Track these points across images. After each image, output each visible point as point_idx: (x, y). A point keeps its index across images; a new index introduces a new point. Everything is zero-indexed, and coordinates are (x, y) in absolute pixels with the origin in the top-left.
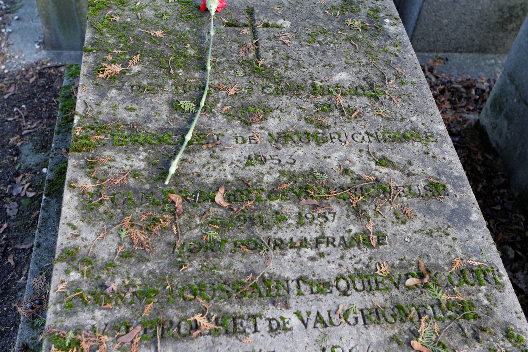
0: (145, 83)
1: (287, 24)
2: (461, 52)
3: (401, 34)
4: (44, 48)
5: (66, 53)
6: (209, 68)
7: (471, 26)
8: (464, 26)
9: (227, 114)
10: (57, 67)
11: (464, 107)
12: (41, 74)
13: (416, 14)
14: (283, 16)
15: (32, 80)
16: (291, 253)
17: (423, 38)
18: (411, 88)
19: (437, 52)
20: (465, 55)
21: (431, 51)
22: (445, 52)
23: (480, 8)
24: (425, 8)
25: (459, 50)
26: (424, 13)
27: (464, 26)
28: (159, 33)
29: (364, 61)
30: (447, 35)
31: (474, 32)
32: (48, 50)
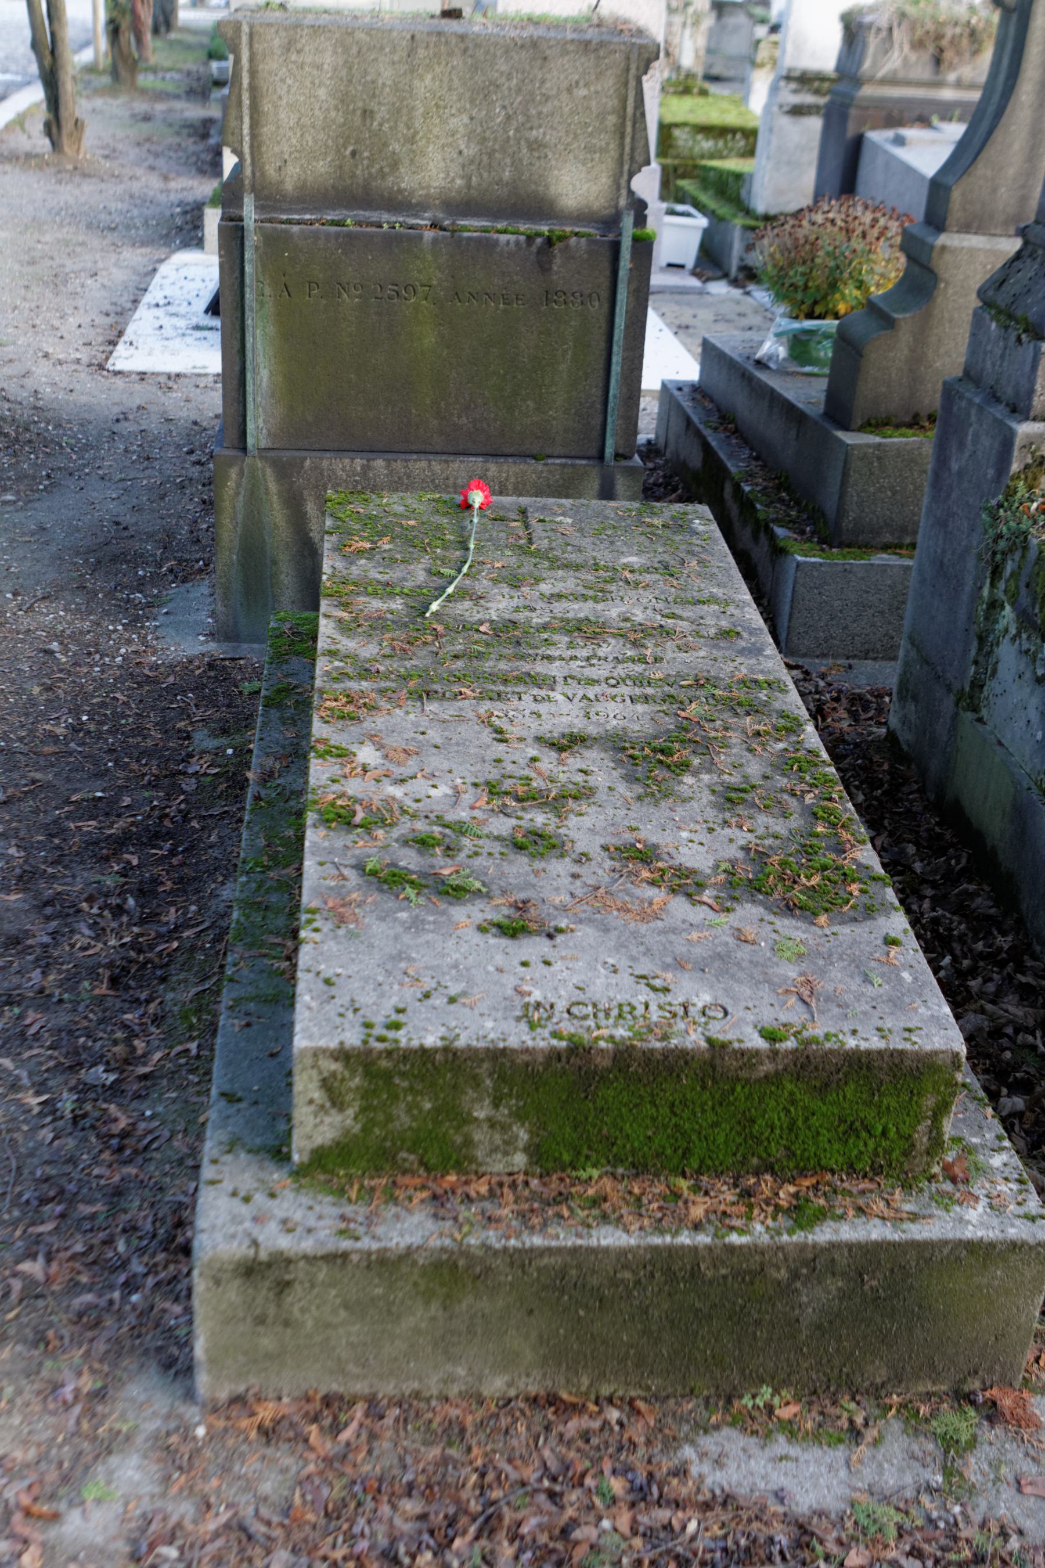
0: (398, 556)
1: (570, 521)
2: (875, 659)
3: (713, 531)
4: (213, 640)
5: (245, 646)
6: (472, 546)
7: (882, 613)
8: (872, 611)
9: (492, 579)
10: (233, 659)
11: (871, 719)
12: (211, 666)
13: (789, 593)
14: (563, 514)
15: (197, 672)
16: (558, 663)
17: (806, 632)
18: (716, 571)
19: (834, 657)
20: (884, 663)
21: (824, 655)
22: (848, 658)
23: (889, 582)
24: (801, 581)
25: (871, 654)
26: (801, 590)
27: (872, 611)
28: (412, 523)
29: (661, 550)
30: (845, 628)
31: (890, 623)
32: (219, 641)
